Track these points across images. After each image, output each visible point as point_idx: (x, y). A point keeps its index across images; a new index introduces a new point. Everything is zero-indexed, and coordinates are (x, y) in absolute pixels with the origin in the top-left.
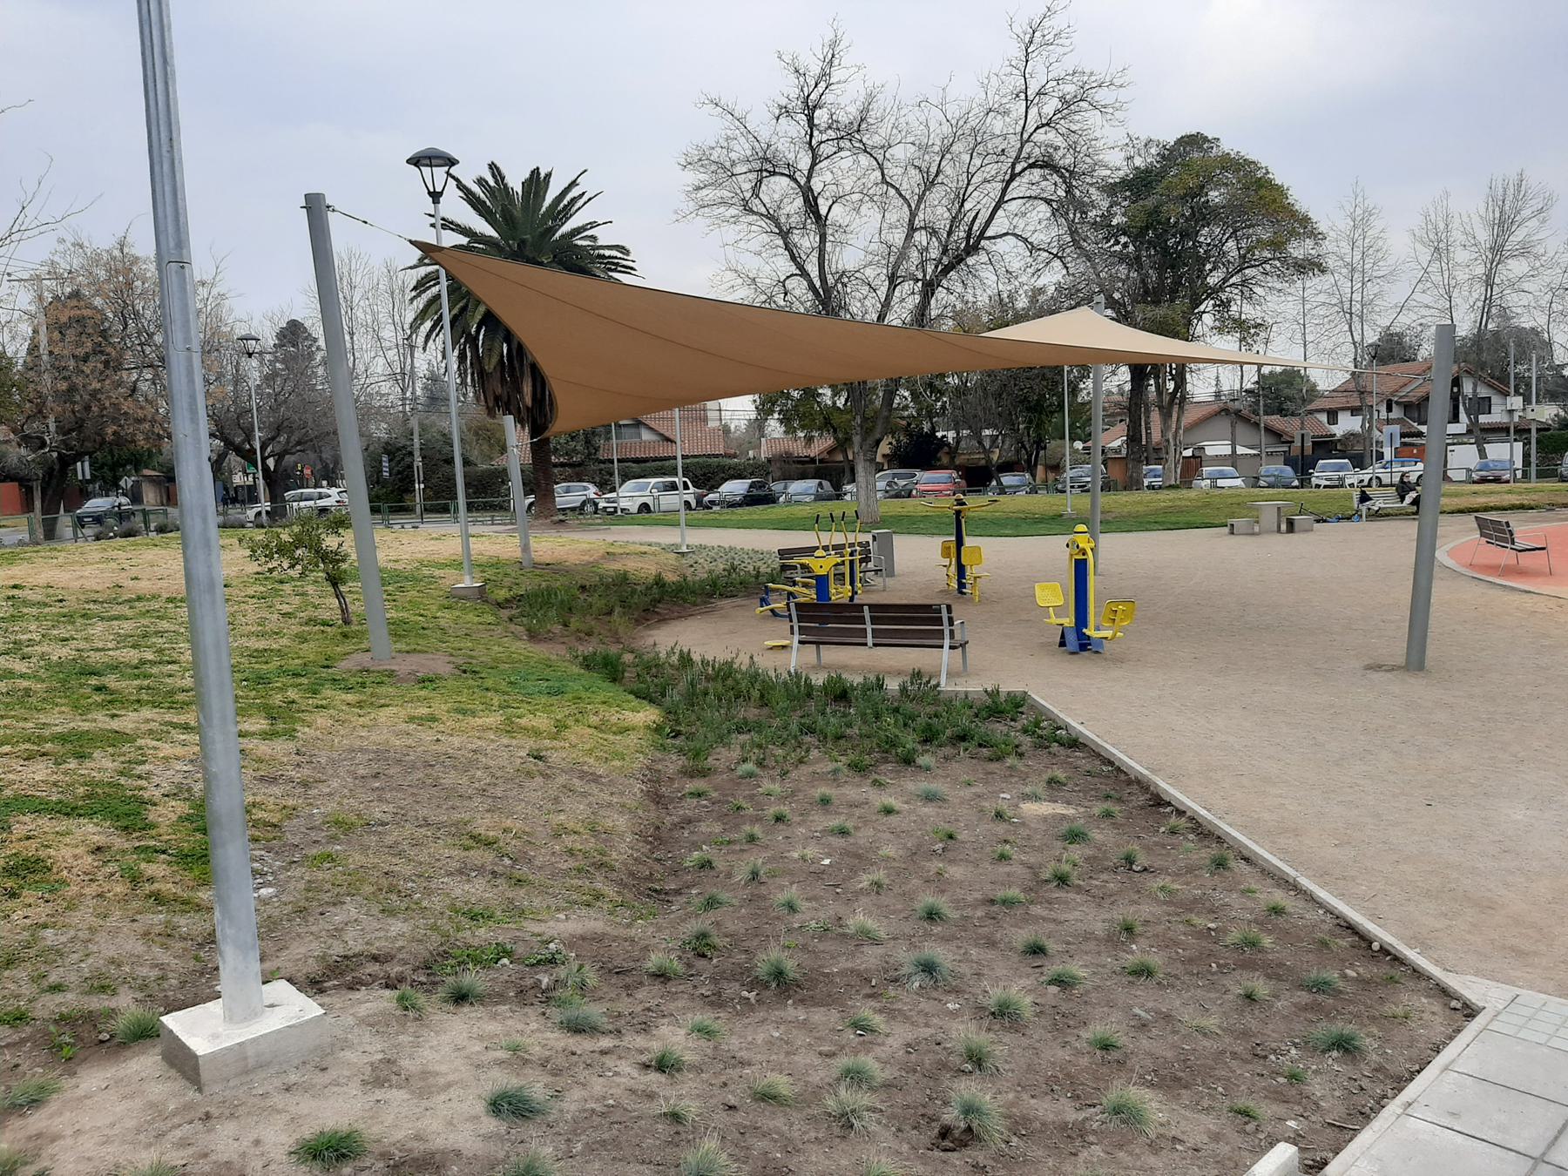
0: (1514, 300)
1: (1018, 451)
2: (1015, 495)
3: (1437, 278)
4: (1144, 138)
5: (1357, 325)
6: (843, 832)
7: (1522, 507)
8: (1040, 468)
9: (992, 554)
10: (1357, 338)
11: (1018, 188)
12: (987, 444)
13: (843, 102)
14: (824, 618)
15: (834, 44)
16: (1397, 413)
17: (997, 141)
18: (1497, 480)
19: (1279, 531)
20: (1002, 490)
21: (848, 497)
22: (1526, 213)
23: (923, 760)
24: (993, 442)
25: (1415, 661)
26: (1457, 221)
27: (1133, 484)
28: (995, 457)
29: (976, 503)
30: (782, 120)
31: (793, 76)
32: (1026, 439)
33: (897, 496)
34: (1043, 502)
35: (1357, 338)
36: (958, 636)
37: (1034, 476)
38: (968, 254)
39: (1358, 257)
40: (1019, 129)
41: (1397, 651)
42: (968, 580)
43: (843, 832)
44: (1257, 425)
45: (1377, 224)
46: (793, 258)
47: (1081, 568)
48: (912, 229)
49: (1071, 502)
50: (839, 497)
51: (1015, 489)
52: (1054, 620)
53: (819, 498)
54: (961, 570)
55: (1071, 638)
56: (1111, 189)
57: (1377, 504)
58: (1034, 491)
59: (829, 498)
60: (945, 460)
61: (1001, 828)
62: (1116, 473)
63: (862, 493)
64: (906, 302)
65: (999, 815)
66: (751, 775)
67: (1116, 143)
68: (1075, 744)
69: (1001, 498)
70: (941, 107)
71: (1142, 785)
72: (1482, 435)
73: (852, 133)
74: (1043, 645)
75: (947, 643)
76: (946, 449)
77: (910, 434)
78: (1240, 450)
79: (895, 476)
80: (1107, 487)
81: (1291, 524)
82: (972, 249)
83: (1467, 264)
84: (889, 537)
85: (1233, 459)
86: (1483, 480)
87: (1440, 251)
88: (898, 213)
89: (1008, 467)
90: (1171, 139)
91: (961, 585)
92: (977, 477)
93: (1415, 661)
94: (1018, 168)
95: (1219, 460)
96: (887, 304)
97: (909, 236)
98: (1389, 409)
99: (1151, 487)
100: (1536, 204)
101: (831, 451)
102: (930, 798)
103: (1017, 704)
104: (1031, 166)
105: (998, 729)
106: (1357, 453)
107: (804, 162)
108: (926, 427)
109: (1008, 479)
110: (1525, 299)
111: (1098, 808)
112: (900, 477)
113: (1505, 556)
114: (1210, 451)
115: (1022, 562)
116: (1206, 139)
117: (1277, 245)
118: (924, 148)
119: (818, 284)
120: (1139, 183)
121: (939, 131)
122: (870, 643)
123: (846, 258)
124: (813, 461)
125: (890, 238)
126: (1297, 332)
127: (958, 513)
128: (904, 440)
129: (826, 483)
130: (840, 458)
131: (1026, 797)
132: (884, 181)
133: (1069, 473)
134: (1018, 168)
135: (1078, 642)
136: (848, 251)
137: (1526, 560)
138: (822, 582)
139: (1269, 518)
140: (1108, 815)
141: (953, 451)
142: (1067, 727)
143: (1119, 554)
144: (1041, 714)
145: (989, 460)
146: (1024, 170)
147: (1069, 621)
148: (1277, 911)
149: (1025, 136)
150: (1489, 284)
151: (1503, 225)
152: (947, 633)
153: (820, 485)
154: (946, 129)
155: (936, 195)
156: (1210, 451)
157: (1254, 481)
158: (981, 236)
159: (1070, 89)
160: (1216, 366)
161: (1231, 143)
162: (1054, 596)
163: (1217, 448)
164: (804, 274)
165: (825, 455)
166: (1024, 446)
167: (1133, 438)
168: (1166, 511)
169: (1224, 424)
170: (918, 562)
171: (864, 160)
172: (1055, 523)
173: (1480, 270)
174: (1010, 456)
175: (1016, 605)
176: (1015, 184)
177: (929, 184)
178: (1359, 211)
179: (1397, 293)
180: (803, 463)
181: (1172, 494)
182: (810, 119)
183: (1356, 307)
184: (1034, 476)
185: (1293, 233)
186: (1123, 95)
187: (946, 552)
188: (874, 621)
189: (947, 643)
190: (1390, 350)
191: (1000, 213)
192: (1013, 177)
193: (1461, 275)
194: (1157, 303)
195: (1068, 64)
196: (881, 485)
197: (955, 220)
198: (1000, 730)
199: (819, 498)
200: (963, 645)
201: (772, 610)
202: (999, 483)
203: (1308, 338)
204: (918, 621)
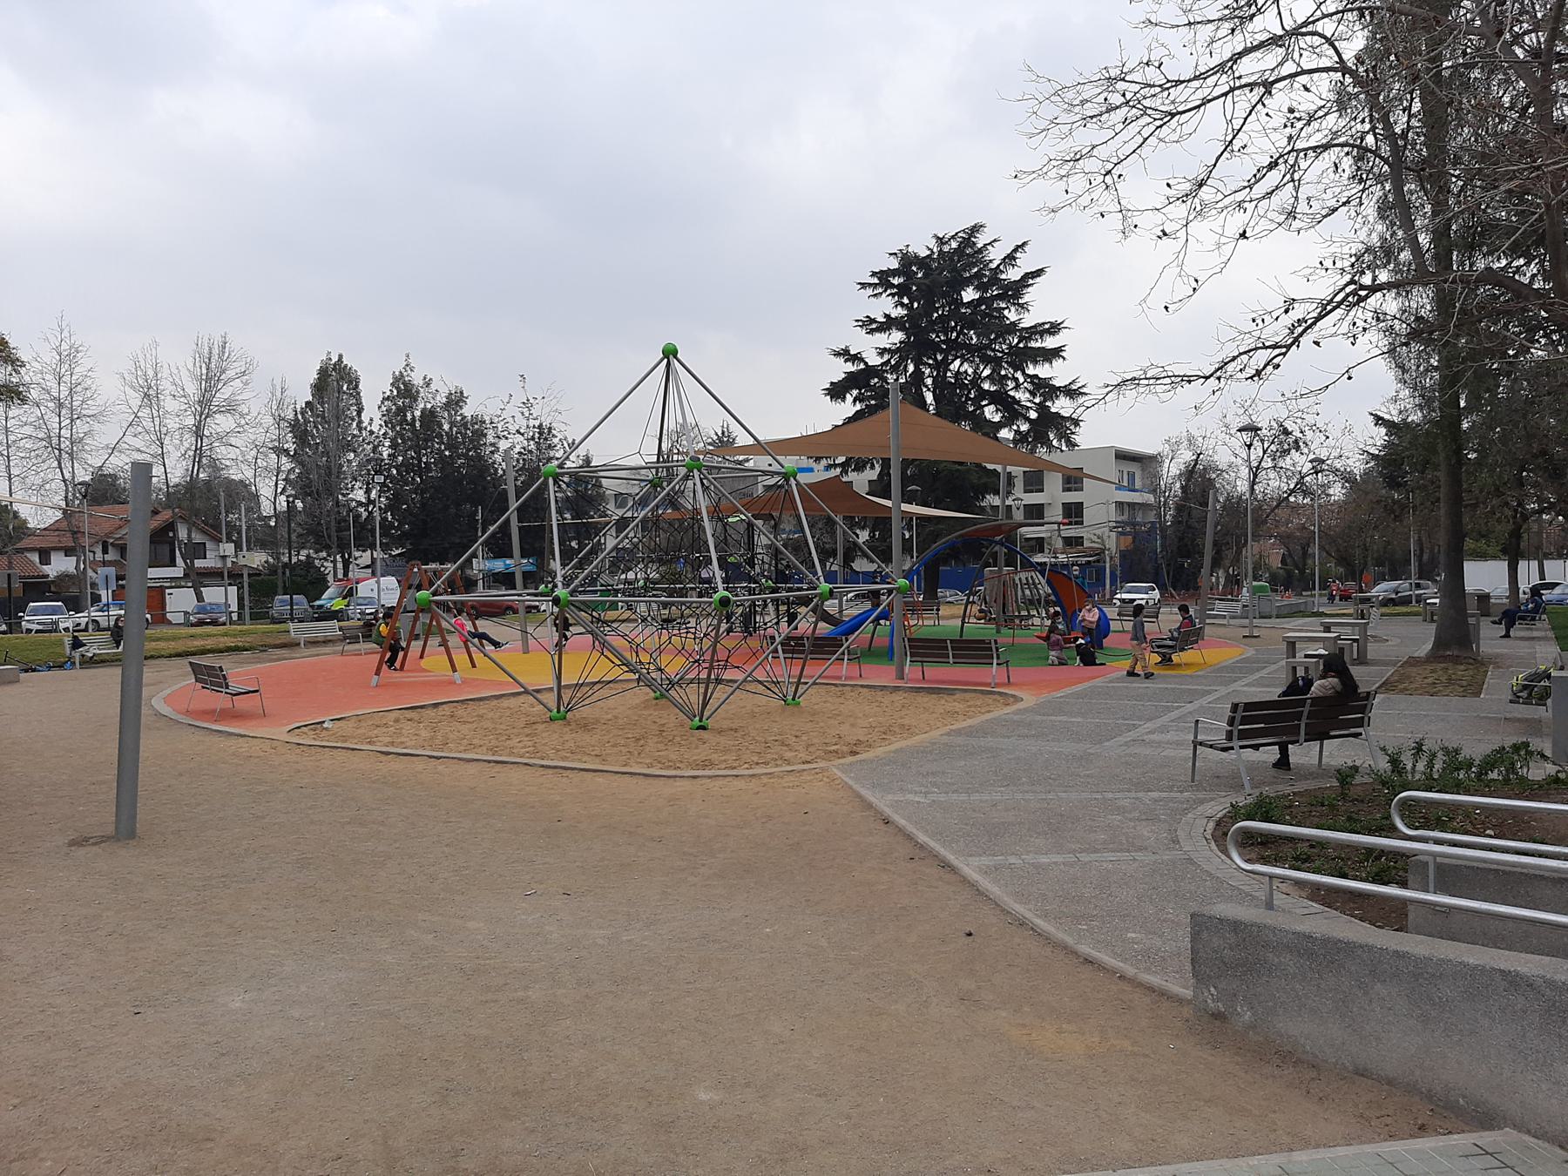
3: (148, 424)
5: (66, 464)
10: (68, 476)
18: (214, 623)
22: (230, 373)
25: (125, 829)
39: (65, 393)
41: (105, 818)
72: (198, 579)
83: (177, 414)
86: (201, 623)
87: (150, 397)
93: (125, 829)
98: (105, 551)
100: (239, 367)
113: (220, 701)
137: (241, 703)
151: (211, 381)
173: (190, 421)
178: (65, 346)
179: (107, 434)
183: (65, 444)
190: (101, 490)
203: (15, 471)
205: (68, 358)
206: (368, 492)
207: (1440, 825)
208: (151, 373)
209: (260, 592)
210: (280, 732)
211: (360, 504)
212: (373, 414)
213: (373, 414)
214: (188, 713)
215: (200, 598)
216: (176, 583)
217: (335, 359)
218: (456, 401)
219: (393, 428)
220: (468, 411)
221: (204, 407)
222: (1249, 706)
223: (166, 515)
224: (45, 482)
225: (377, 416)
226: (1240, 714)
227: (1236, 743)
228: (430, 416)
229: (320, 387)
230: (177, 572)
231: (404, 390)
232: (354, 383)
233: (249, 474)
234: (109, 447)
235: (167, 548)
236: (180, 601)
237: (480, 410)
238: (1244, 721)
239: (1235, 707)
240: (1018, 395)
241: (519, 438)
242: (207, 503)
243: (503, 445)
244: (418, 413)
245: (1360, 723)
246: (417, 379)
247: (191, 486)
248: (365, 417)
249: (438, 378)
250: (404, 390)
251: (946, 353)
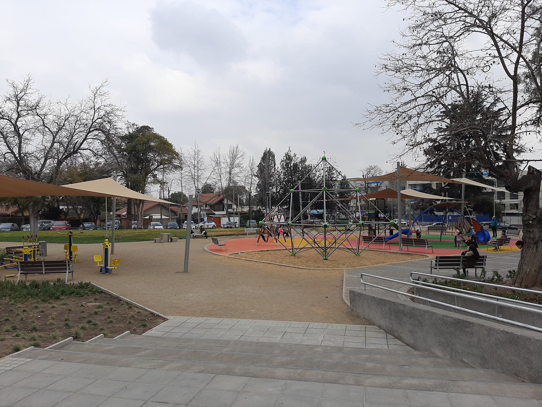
0: (236, 179)
1: (90, 215)
2: (89, 229)
3: (217, 171)
4: (132, 123)
5: (196, 183)
6: (43, 312)
7: (223, 235)
8: (98, 221)
9: (80, 249)
10: (196, 186)
11: (90, 135)
12: (79, 212)
13: (31, 99)
14: (28, 266)
15: (29, 80)
16: (208, 208)
17: (84, 121)
18: (231, 228)
19: (168, 241)
20: (84, 228)
21: (24, 230)
22: (239, 156)
23: (61, 298)
24: (81, 212)
25: (186, 271)
26: (222, 157)
27: (129, 227)
28: (82, 217)
29: (76, 232)
30: (7, 102)
31: (12, 89)
32: (93, 212)
33: (44, 230)
34: (99, 233)
35: (196, 186)
36: (71, 270)
37: (96, 224)
38: (74, 154)
39: (196, 163)
40: (92, 118)
41: (182, 269)
42: (73, 256)
43: (43, 312)
44: (168, 209)
45: (201, 154)
46: (8, 146)
47: (106, 250)
48: (53, 142)
49: (107, 233)
50: (19, 230)
51: (89, 228)
52: (99, 265)
53: (12, 230)
54: (71, 253)
55: (103, 270)
56: (123, 138)
57: (195, 234)
58: (96, 229)
59: (17, 230)
60: (63, 217)
61: (82, 308)
62: (124, 223)
63: (32, 228)
64: (51, 163)
65: (82, 306)
66: (13, 304)
67: (122, 127)
68: (102, 292)
69: (84, 231)
70: (66, 105)
71: (117, 298)
72: (229, 215)
73: (33, 109)
74: (95, 272)
75: (68, 271)
76: (63, 213)
77: (49, 208)
78: (163, 217)
79: (43, 222)
80: (120, 228)
81: (171, 239)
82: (76, 152)
83: (225, 168)
84: (45, 243)
85: (161, 220)
86: (228, 228)
87: (218, 163)
88: (49, 137)
89: (87, 220)
90: (140, 125)
91: (71, 258)
92: (75, 223)
93: (186, 271)
94: (91, 130)
95: (157, 220)
96: (43, 165)
97: (52, 145)
98: (206, 207)
99: (134, 228)
100: (241, 154)
101: (16, 212)
102: (64, 304)
103: (87, 285)
104: (96, 130)
105: (82, 291)
106: (196, 219)
107: (15, 116)
108: (56, 205)
109: (86, 225)
110: (239, 179)
111: (106, 303)
112: (45, 223)
113: (217, 247)
114: (154, 217)
115: (90, 251)
116: (150, 128)
117: (170, 162)
118: (59, 117)
119: (17, 156)
120: (129, 138)
121: (64, 112)
122: (44, 272)
123: (28, 148)
124: (8, 215)
125: (46, 144)
126: (177, 182)
127: (70, 236)
128: (47, 209)
129: (15, 225)
130: (21, 215)
131: (89, 302)
132: (44, 125)
133: (107, 223)
134: (91, 130)
135: (105, 271)
136: (29, 146)
137: (223, 248)
138: (26, 256)
139: (165, 238)
140: (108, 303)
141: (66, 214)
142: (100, 289)
143: (121, 248)
144: (93, 287)
145: (80, 218)
146: (93, 130)
147: (103, 265)
148: (139, 312)
149: (94, 121)
150: (230, 174)
151: (234, 157)
152: (68, 268)
153: (13, 225)
154: (67, 112)
155: (63, 133)
156: (154, 217)
157: (166, 227)
158: (79, 148)
159: (108, 109)
160: (153, 193)
161: (157, 130)
162: (99, 259)
163: (156, 216)
164: (12, 152)
165: (14, 214)
166: (92, 213)
167: (129, 212)
168: (138, 236)
169: (158, 209)
170: (56, 251)
171: (37, 118)
172: (101, 239)
173: (228, 170)
174: (87, 216)
175: (88, 263)
176: (90, 134)
177: (60, 129)
178: (196, 150)
179: (207, 174)
180: (3, 216)
181: (139, 231)
182: (18, 103)
183: (196, 177)
184: (96, 224)
185: (174, 158)
186: (124, 113)
187: (65, 248)
188: (45, 266)
189: (68, 271)
190: (208, 189)
191: (85, 142)
192: (90, 132)
193: (223, 171)
194: (135, 173)
195: (108, 102)
196: (39, 225)
197: (69, 142)
198: (84, 290)
199: (12, 230)
200: (72, 272)
201: (5, 267)
202: (83, 226)
203: (183, 185)
204: (58, 266)
205: (197, 153)
206: (277, 189)
207: (531, 300)
208: (218, 156)
209: (245, 218)
210: (227, 255)
211: (274, 193)
212: (278, 165)
213: (278, 165)
214: (211, 250)
215: (229, 220)
216: (224, 216)
217: (268, 150)
218: (304, 160)
219: (285, 170)
220: (307, 163)
221: (232, 166)
222: (440, 258)
223: (222, 197)
224: (191, 188)
225: (279, 166)
226: (438, 259)
227: (438, 267)
228: (296, 165)
229: (263, 159)
230: (225, 213)
231: (288, 158)
232: (273, 157)
233: (243, 185)
234: (208, 176)
235: (222, 206)
236: (224, 221)
237: (311, 163)
238: (440, 261)
239: (437, 257)
240: (498, 152)
241: (322, 171)
242: (233, 192)
243: (318, 173)
244: (292, 165)
245: (482, 264)
246: (292, 154)
247: (228, 189)
248: (276, 167)
249: (298, 154)
250: (288, 158)
251: (469, 138)
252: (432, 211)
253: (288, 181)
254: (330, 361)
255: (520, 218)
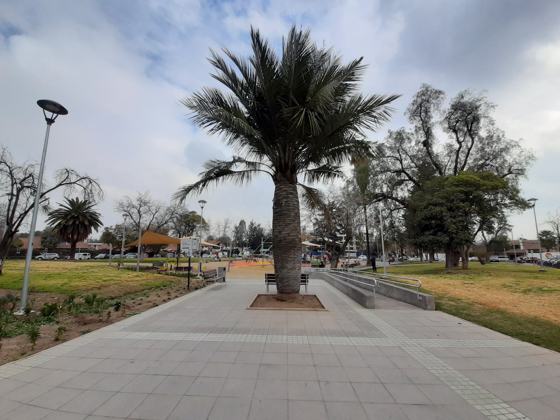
0: (227, 234)
83: (222, 228)
87: (219, 226)
151: (226, 224)
218: (259, 225)
220: (261, 227)
221: (225, 227)
222: (269, 275)
228: (255, 227)
229: (240, 224)
231: (252, 224)
238: (268, 278)
249: (256, 223)
250: (252, 224)
252: (317, 250)
253: (251, 235)
254: (476, 227)
255: (355, 254)
